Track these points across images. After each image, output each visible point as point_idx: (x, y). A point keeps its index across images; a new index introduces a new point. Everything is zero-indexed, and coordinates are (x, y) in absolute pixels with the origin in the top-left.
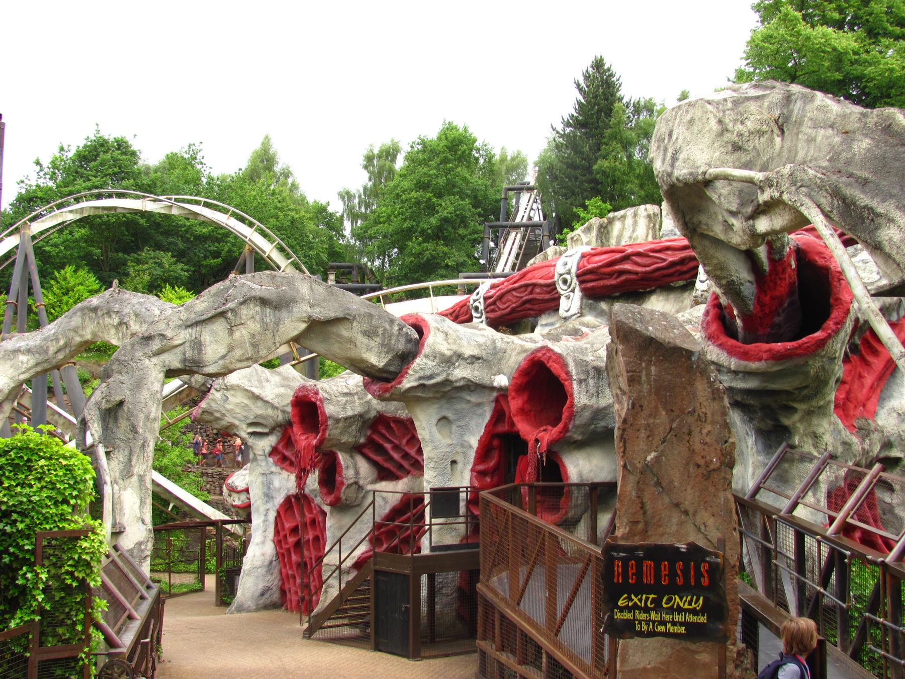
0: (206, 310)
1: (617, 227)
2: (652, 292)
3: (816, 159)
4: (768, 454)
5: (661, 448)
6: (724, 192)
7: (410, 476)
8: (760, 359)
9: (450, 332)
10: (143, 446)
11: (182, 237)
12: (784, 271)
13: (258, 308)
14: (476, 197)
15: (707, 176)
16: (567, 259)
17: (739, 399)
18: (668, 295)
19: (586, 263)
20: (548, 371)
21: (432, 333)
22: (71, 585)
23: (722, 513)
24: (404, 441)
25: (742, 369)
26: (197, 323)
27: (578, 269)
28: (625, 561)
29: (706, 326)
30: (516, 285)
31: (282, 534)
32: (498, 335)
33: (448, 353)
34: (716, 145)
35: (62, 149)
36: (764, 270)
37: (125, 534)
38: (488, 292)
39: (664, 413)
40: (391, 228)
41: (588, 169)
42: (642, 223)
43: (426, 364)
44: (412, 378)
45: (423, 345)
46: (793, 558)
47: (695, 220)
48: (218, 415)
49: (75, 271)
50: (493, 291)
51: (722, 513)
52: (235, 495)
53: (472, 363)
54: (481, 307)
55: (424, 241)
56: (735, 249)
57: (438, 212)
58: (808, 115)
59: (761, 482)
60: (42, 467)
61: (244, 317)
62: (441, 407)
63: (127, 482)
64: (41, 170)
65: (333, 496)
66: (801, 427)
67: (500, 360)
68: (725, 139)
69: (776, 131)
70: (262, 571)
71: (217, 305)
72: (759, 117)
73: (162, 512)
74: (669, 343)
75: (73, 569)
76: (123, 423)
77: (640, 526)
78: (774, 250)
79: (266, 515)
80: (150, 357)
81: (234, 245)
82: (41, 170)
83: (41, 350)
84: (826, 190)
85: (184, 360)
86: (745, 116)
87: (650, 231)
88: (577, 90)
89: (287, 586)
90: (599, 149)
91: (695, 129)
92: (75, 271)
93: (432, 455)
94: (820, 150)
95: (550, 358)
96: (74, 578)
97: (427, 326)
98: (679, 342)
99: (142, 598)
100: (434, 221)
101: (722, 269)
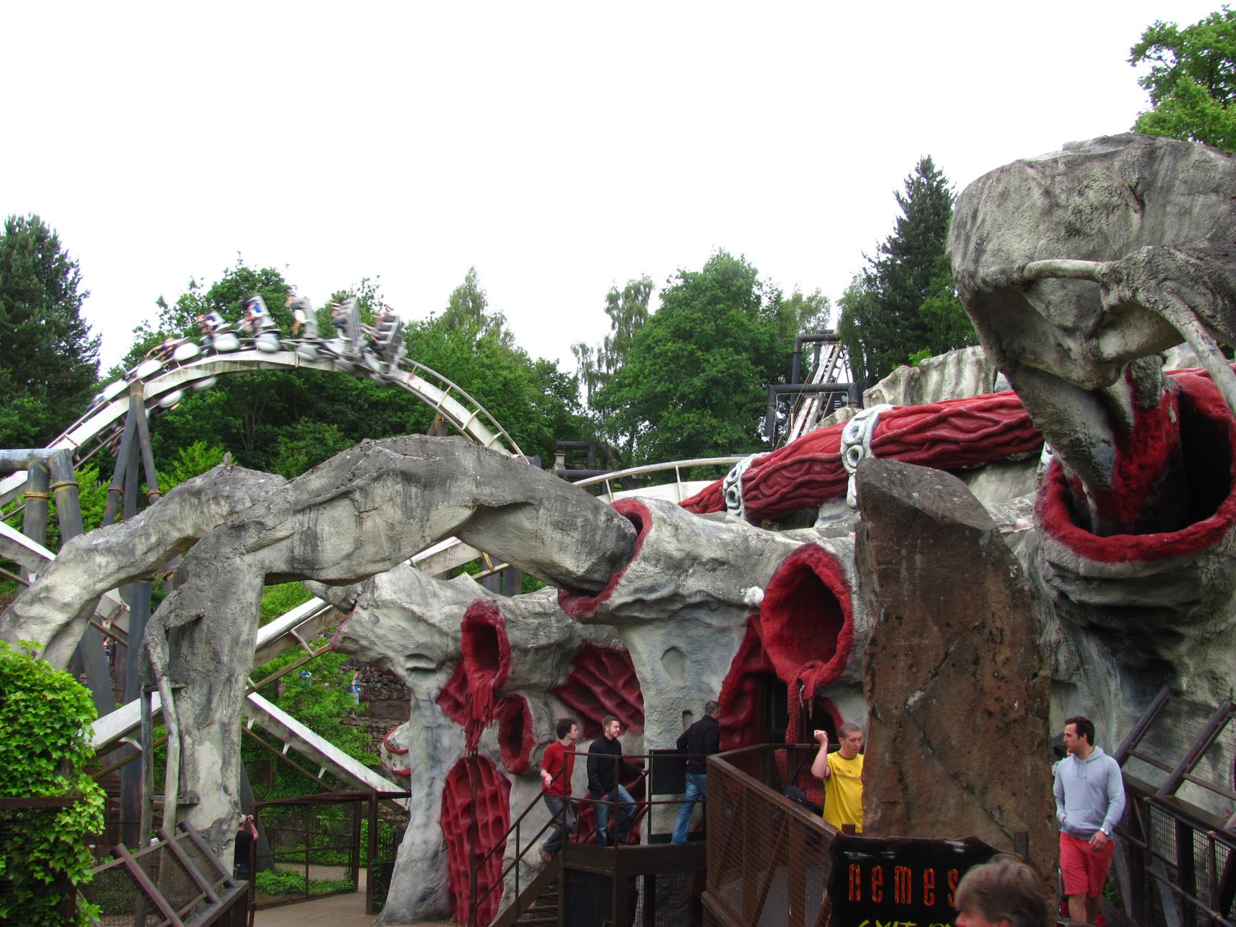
0: (325, 489)
1: (934, 377)
2: (980, 470)
3: (1191, 240)
4: (1140, 703)
5: (931, 684)
6: (1055, 298)
8: (1122, 559)
9: (682, 524)
10: (229, 680)
11: (353, 404)
12: (1158, 425)
13: (399, 487)
14: (757, 350)
15: (1026, 274)
16: (859, 423)
17: (1095, 620)
18: (1003, 473)
19: (885, 429)
20: (816, 579)
21: (655, 526)
22: (42, 881)
23: (1029, 791)
24: (620, 683)
25: (1095, 574)
26: (311, 507)
27: (874, 436)
28: (866, 866)
29: (1040, 511)
30: (788, 461)
31: (452, 813)
32: (752, 530)
33: (678, 555)
34: (1041, 228)
35: (193, 285)
36: (1128, 425)
37: (198, 807)
38: (747, 471)
39: (935, 629)
40: (640, 392)
41: (912, 311)
42: (969, 373)
43: (645, 570)
45: (641, 542)
46: (1175, 863)
47: (1016, 346)
49: (207, 449)
50: (755, 470)
51: (1029, 791)
52: (396, 757)
53: (714, 570)
55: (685, 410)
56: (1077, 388)
57: (703, 371)
58: (1181, 176)
59: (1129, 746)
60: (16, 702)
61: (378, 499)
62: (669, 634)
63: (204, 732)
64: (166, 313)
65: (518, 760)
66: (1191, 663)
67: (755, 565)
68: (1055, 219)
69: (1133, 204)
70: (421, 865)
72: (1106, 184)
73: (312, 780)
74: (944, 517)
75: (48, 857)
76: (201, 648)
77: (899, 809)
78: (1142, 393)
79: (430, 786)
80: (242, 554)
81: (423, 415)
82: (166, 313)
83: (125, 550)
84: (1205, 283)
85: (292, 560)
86: (1085, 183)
87: (981, 385)
88: (897, 203)
89: (457, 888)
90: (927, 283)
91: (1010, 205)
92: (207, 449)
93: (655, 702)
94: (1198, 224)
95: (820, 560)
96: (47, 870)
97: (648, 516)
98: (959, 517)
99: (208, 900)
100: (698, 382)
101: (1061, 421)
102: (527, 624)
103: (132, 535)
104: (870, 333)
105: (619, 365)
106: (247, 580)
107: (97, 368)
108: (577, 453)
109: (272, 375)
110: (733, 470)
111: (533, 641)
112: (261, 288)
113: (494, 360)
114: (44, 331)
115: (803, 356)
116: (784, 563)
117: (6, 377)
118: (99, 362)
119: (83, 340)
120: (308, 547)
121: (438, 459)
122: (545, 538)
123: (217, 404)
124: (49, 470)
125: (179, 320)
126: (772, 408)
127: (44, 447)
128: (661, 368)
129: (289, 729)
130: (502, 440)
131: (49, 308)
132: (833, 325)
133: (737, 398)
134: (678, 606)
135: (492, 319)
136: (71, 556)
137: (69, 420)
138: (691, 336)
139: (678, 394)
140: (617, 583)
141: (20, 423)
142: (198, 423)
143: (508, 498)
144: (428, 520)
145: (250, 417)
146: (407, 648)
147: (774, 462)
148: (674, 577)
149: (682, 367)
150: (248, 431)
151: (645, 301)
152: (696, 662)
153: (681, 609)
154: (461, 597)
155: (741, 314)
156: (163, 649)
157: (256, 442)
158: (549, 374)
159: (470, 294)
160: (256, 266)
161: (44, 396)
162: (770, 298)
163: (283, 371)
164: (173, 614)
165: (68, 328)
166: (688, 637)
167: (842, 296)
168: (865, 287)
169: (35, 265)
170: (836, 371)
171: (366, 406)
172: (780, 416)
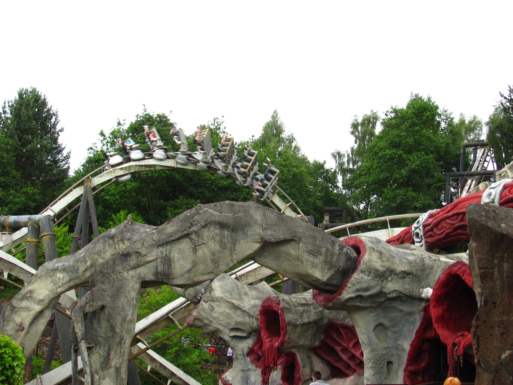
0: (175, 233)
7: (355, 374)
10: (120, 342)
11: (209, 188)
13: (217, 231)
14: (438, 152)
16: (492, 190)
19: (508, 194)
21: (368, 252)
24: (351, 345)
27: (501, 198)
30: (450, 214)
32: (427, 255)
33: (381, 269)
35: (119, 124)
38: (426, 220)
40: (371, 179)
44: (351, 290)
45: (360, 262)
48: (206, 321)
50: (431, 220)
53: (403, 278)
54: (421, 233)
55: (397, 188)
57: (407, 165)
61: (205, 238)
62: (377, 315)
67: (428, 275)
71: (184, 228)
76: (104, 324)
80: (128, 270)
82: (104, 139)
85: (157, 273)
95: (464, 271)
97: (364, 246)
100: (404, 172)
102: (296, 310)
103: (77, 261)
104: (506, 141)
105: (360, 164)
106: (131, 285)
107: (68, 171)
108: (337, 214)
109: (163, 173)
110: (418, 220)
111: (300, 320)
112: (156, 124)
113: (288, 162)
114: (39, 151)
115: (466, 156)
116: (443, 273)
117: (19, 176)
118: (69, 167)
119: (60, 155)
120: (166, 266)
121: (240, 215)
122: (303, 260)
123: (133, 190)
124: (39, 227)
125: (111, 143)
126: (448, 186)
127: (37, 214)
128: (382, 164)
129: (171, 371)
130: (291, 206)
131: (42, 138)
132: (484, 137)
133: (427, 181)
134: (382, 299)
135: (287, 139)
136: (43, 273)
137: (52, 198)
138: (400, 146)
139: (393, 179)
140: (346, 286)
141: (26, 201)
142: (123, 200)
143: (281, 236)
144: (234, 250)
145: (152, 196)
146: (230, 325)
147: (441, 215)
148: (380, 282)
149: (395, 164)
150: (151, 204)
151: (374, 127)
152: (394, 332)
153: (384, 301)
154: (261, 295)
155: (430, 133)
156: (82, 325)
157: (155, 210)
158: (320, 169)
159: (274, 126)
160: (154, 112)
161: (39, 187)
162: (445, 123)
163: (169, 170)
164: (88, 305)
165: (52, 149)
166: (389, 318)
167: (488, 120)
168: (503, 114)
169: (34, 115)
170: (486, 164)
171: (216, 189)
172: (452, 190)
